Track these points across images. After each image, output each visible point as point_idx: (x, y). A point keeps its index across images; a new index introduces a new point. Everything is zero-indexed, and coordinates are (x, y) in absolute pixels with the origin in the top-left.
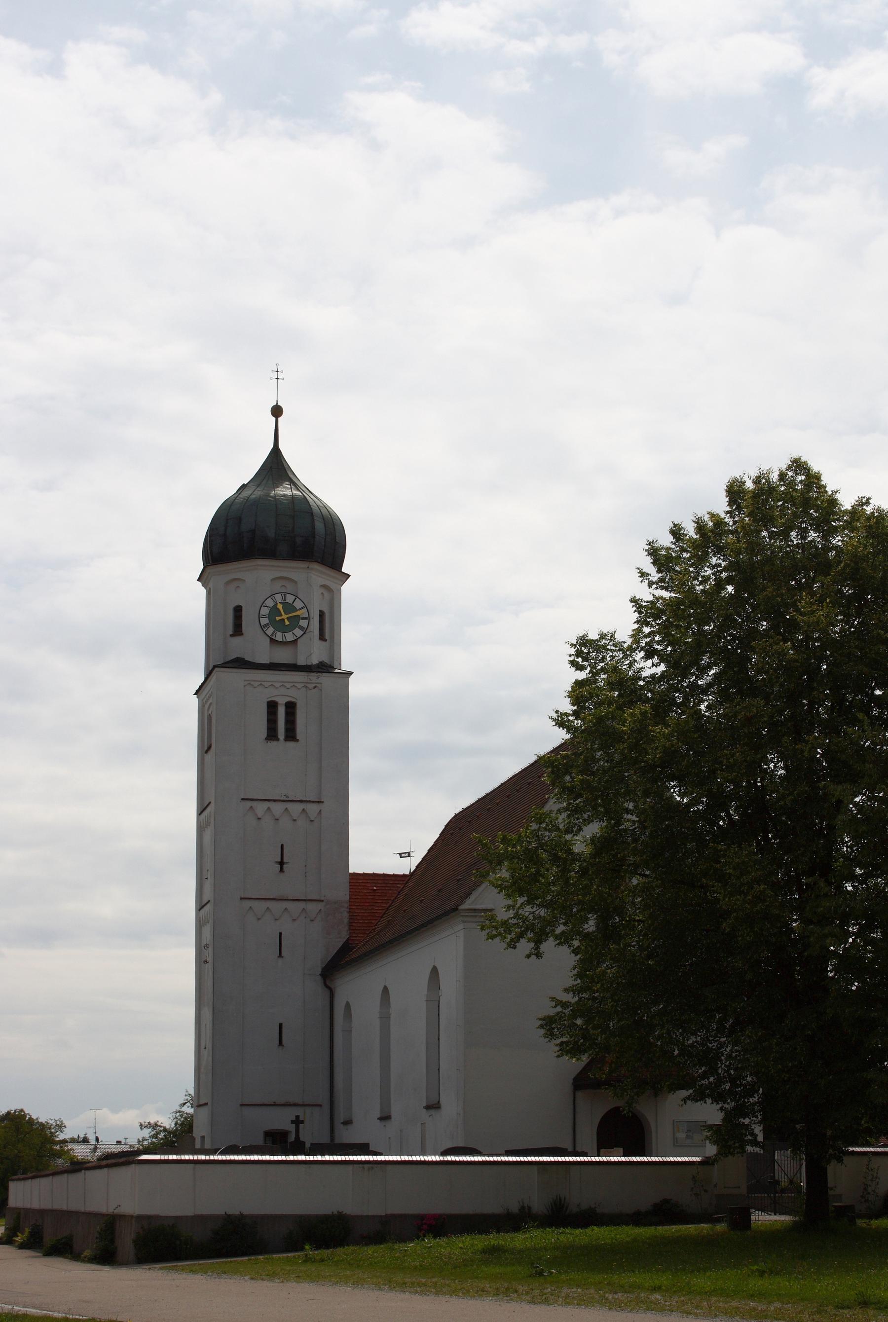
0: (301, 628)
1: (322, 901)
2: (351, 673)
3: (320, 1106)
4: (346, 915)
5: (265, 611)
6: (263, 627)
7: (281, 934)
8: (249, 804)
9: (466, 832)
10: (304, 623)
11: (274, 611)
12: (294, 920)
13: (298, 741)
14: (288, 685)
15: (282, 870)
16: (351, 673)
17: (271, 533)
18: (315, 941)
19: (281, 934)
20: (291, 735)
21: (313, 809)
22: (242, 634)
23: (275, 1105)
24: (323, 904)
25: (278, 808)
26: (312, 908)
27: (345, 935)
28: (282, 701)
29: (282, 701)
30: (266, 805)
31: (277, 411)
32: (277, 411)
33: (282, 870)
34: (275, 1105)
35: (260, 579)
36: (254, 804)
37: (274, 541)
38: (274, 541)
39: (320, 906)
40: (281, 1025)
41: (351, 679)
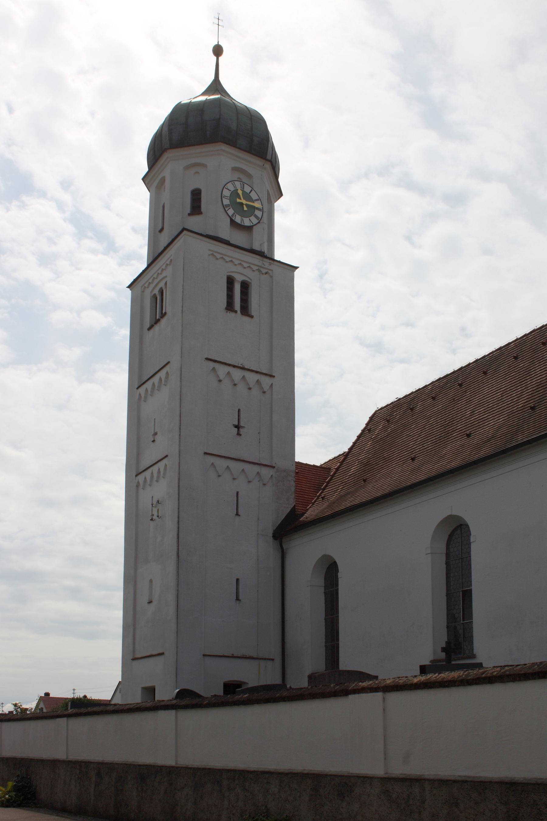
0: (256, 217)
1: (274, 467)
2: (297, 268)
3: (273, 660)
4: (293, 483)
5: (226, 193)
6: (224, 207)
7: (237, 493)
8: (212, 364)
9: (390, 424)
10: (258, 213)
11: (235, 194)
12: (249, 482)
13: (252, 317)
14: (246, 265)
15: (239, 434)
16: (297, 268)
17: (234, 127)
18: (267, 505)
19: (237, 493)
20: (245, 310)
21: (266, 381)
22: (200, 213)
23: (233, 657)
24: (275, 470)
25: (237, 374)
26: (266, 473)
27: (292, 503)
28: (239, 278)
29: (239, 278)
30: (227, 369)
31: (218, 51)
32: (218, 51)
33: (239, 434)
34: (233, 657)
35: (219, 165)
36: (217, 365)
37: (213, 155)
38: (213, 155)
39: (271, 472)
40: (238, 580)
41: (296, 273)
